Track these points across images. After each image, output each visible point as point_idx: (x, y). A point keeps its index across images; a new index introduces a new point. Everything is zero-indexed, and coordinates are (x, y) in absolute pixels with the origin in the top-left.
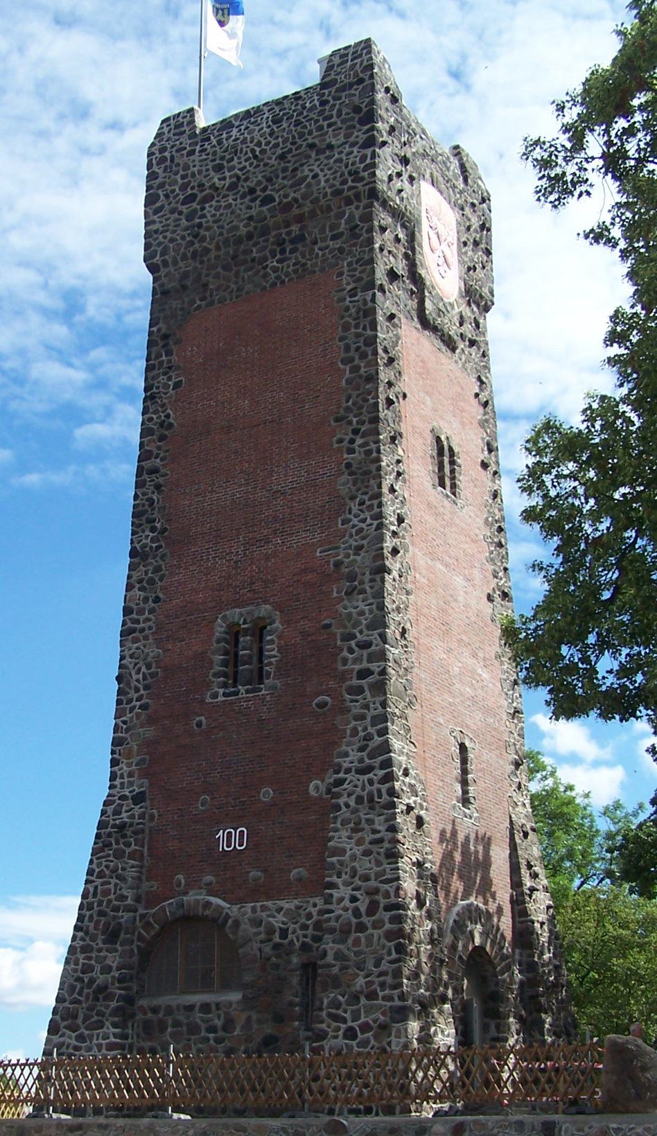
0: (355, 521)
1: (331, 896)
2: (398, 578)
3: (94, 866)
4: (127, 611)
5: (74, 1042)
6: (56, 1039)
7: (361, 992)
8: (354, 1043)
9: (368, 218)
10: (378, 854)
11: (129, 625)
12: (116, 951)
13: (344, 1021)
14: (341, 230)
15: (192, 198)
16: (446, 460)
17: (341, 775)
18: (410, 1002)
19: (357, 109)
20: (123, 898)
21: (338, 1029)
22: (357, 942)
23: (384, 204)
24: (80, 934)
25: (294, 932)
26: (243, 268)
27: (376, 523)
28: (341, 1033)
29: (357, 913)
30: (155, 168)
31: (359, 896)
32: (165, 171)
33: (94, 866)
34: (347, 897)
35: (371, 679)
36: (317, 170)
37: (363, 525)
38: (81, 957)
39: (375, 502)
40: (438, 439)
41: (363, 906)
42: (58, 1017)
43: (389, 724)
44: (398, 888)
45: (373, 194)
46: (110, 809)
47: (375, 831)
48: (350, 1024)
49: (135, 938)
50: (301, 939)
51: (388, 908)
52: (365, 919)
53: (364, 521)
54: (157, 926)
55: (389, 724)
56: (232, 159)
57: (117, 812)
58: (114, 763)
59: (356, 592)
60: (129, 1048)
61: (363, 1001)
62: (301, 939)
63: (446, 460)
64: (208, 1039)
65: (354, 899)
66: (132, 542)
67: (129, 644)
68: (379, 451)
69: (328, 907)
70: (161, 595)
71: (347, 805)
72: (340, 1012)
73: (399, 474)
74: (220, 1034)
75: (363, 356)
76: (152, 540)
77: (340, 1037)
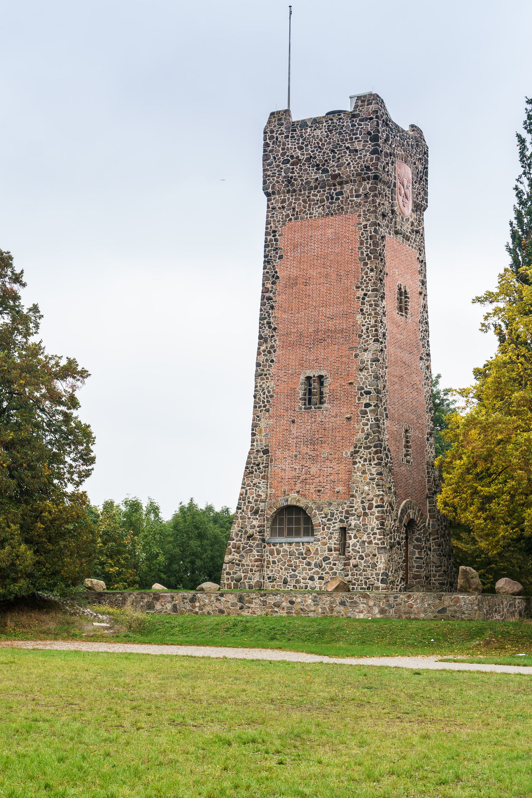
8: (363, 561)
13: (359, 552)
17: (357, 449)
25: (337, 514)
29: (364, 508)
30: (268, 141)
41: (366, 505)
47: (371, 474)
48: (361, 554)
52: (367, 511)
61: (366, 544)
62: (340, 518)
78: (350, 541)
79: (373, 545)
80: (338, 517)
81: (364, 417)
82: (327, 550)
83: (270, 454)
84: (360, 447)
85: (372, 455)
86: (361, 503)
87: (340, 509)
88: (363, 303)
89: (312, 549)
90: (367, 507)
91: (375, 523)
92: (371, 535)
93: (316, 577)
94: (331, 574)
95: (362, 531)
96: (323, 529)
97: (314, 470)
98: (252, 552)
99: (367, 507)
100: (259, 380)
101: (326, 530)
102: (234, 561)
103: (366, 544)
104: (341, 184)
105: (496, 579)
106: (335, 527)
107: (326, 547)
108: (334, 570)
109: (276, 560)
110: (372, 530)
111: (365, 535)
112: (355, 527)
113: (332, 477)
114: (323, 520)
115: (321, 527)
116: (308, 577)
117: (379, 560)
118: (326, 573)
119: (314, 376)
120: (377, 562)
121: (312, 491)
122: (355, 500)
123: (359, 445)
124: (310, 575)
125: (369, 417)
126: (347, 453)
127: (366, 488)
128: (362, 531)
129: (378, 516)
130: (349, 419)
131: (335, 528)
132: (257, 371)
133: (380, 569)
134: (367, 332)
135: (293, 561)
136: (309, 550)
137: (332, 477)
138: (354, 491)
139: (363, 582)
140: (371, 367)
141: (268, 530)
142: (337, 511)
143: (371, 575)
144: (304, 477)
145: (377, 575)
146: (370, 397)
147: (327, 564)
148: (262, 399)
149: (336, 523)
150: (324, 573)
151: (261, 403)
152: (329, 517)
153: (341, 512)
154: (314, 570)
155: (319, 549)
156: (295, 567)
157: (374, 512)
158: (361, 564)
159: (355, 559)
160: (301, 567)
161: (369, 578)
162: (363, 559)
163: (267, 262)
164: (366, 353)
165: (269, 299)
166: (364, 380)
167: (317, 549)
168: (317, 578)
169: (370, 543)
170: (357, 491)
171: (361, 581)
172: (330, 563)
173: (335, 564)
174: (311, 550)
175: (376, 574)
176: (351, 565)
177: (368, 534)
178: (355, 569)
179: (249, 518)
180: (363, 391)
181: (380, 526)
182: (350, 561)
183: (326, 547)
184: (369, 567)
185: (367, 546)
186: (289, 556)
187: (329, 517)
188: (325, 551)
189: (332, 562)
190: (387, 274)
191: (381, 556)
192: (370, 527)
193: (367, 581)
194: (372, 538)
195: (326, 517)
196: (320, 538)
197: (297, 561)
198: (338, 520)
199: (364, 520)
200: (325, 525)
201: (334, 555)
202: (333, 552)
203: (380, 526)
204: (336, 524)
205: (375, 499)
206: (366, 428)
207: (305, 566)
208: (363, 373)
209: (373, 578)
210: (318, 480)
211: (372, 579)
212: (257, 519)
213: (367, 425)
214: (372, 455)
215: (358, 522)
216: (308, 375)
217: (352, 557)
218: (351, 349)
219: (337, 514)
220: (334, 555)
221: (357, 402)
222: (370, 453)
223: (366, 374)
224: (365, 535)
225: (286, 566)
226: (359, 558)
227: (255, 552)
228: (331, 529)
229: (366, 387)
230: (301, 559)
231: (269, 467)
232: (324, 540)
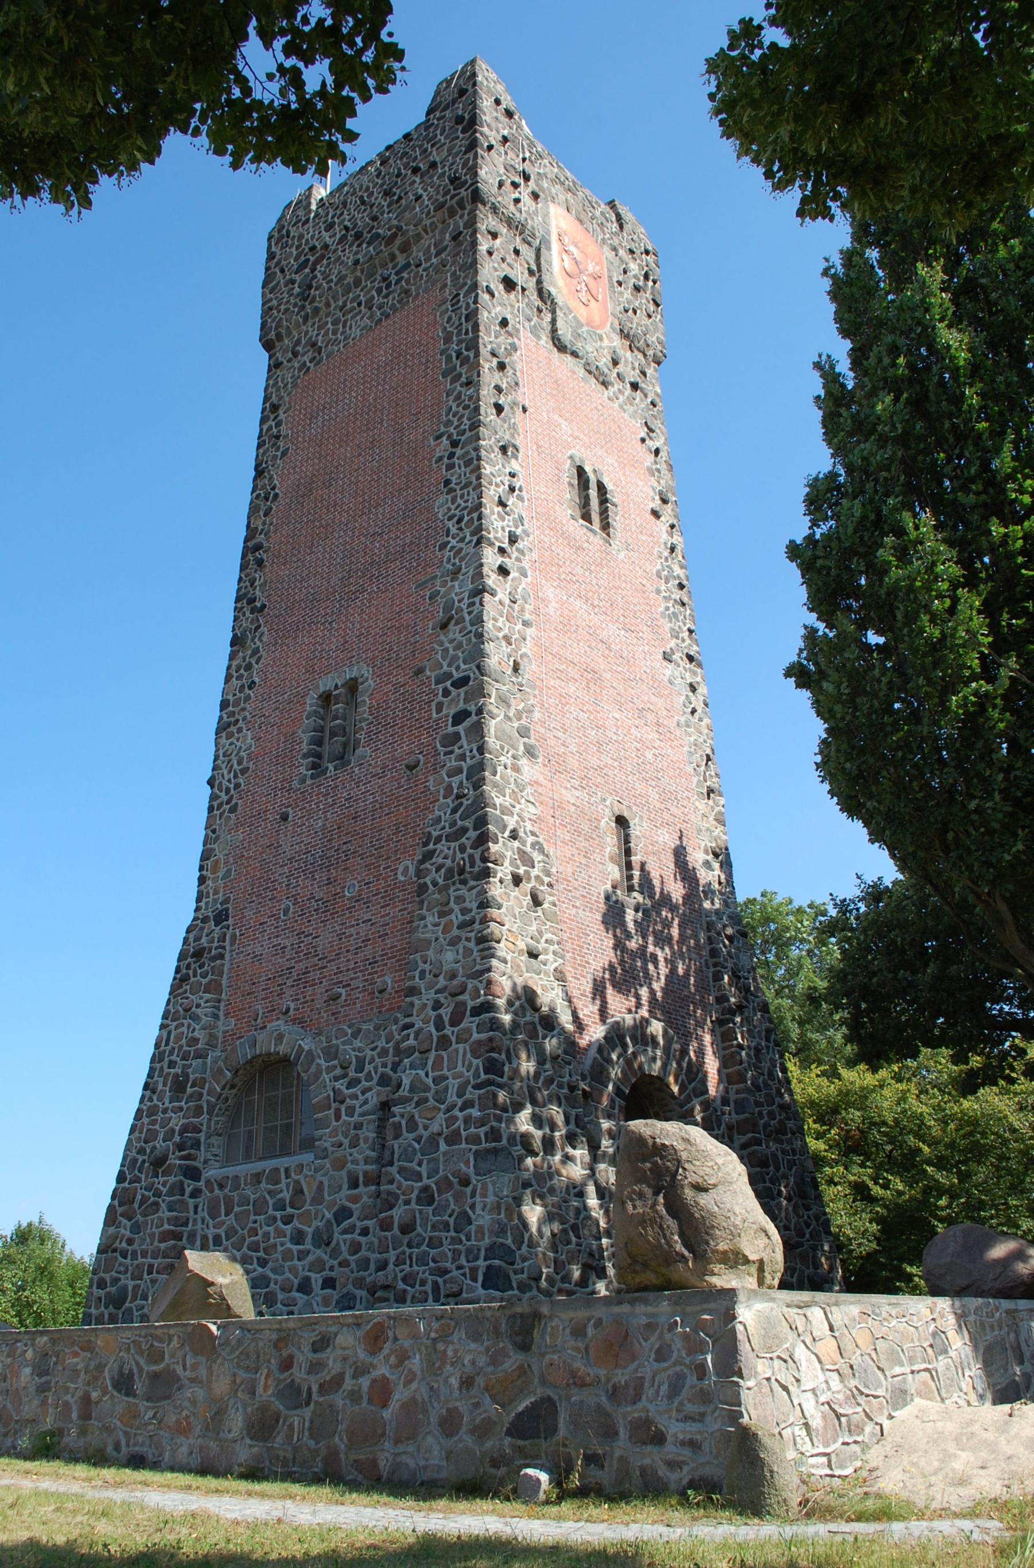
0: (453, 542)
1: (412, 1004)
2: (507, 602)
3: (171, 1007)
4: (224, 705)
5: (128, 1234)
6: (112, 1230)
7: (440, 1134)
8: (430, 1209)
9: (472, 224)
10: (468, 939)
11: (225, 719)
12: (181, 1109)
13: (419, 1177)
14: (446, 243)
15: (305, 264)
16: (593, 493)
17: (431, 846)
18: (504, 1141)
19: (459, 120)
20: (196, 1040)
21: (412, 1189)
22: (438, 1064)
23: (495, 209)
24: (148, 1093)
25: (372, 1060)
26: (349, 316)
27: (475, 539)
28: (414, 1196)
29: (439, 1025)
30: (273, 249)
31: (443, 1000)
32: (282, 248)
33: (171, 1007)
34: (430, 1004)
35: (467, 723)
36: (420, 191)
37: (461, 545)
38: (146, 1120)
39: (475, 515)
40: (581, 471)
41: (446, 1013)
42: (116, 1202)
43: (487, 774)
44: (489, 983)
45: (477, 197)
46: (191, 936)
47: (464, 911)
48: (426, 1181)
49: (205, 1092)
50: (380, 1070)
51: (477, 1011)
52: (448, 1031)
53: (462, 540)
54: (228, 1073)
55: (487, 774)
56: (342, 214)
57: (197, 939)
58: (202, 880)
59: (453, 622)
60: (188, 1237)
61: (443, 1146)
62: (380, 1070)
63: (593, 493)
64: (275, 1219)
65: (437, 1005)
66: (234, 629)
67: (223, 741)
68: (479, 458)
69: (408, 1020)
70: (256, 680)
71: (435, 884)
72: (414, 1165)
73: (512, 489)
74: (289, 1210)
75: (465, 361)
76: (252, 622)
77: (414, 1201)
78: (396, 1144)
79: (464, 1145)
80: (376, 1068)
81: (451, 752)
82: (345, 1186)
83: (231, 921)
84: (438, 840)
85: (469, 851)
86: (434, 1009)
87: (382, 1043)
88: (450, 467)
89: (309, 1184)
90: (446, 1019)
91: (470, 1065)
92: (456, 1112)
93: (316, 1279)
94: (353, 1265)
95: (432, 1102)
96: (338, 1117)
97: (325, 942)
98: (157, 1211)
99: (446, 1019)
100: (223, 741)
101: (344, 1117)
102: (117, 1244)
103: (443, 1146)
104: (405, 248)
105: (1024, 546)
106: (366, 1102)
107: (344, 1173)
108: (364, 1253)
109: (221, 1231)
110: (460, 1095)
111: (441, 1115)
112: (412, 1089)
113: (368, 952)
114: (338, 1085)
115: (332, 1111)
116: (296, 1282)
117: (478, 1199)
118: (340, 1264)
119: (336, 687)
120: (473, 1207)
121: (319, 1004)
122: (417, 1002)
123: (435, 834)
124: (301, 1273)
125: (465, 746)
126: (406, 869)
127: (449, 956)
128: (432, 1102)
129: (479, 1042)
130: (411, 768)
131: (366, 1108)
132: (221, 718)
133: (480, 1230)
134: (461, 529)
135: (260, 1232)
136: (302, 1192)
137: (368, 952)
138: (417, 973)
139: (428, 1288)
140: (470, 613)
141: (214, 1140)
142: (373, 1050)
143: (454, 1260)
144: (302, 965)
145: (472, 1254)
146: (466, 693)
147: (345, 1232)
148: (225, 783)
149: (370, 1089)
150: (336, 1263)
151: (223, 794)
152: (352, 1074)
153: (384, 1053)
154: (310, 1258)
155: (326, 1184)
156: (265, 1250)
157: (469, 1030)
158: (425, 1220)
159: (407, 1202)
160: (280, 1249)
161: (446, 1272)
162: (431, 1201)
163: (260, 471)
164: (456, 583)
165: (258, 547)
166: (451, 652)
167: (321, 1183)
168: (320, 1282)
169: (453, 1139)
170: (423, 973)
171: (423, 1283)
172: (350, 1230)
173: (365, 1232)
174: (305, 1190)
175: (469, 1251)
176: (396, 1229)
177: (448, 1110)
178: (406, 1239)
179: (165, 1111)
180: (448, 684)
181: (483, 1076)
182: (394, 1211)
183: (344, 1173)
184: (446, 1226)
185: (445, 1154)
186: (252, 1218)
187: (352, 1074)
188: (340, 1187)
189: (359, 1224)
190: (525, 410)
191: (485, 1186)
192: (453, 1084)
193: (440, 1280)
194: (460, 1123)
195: (345, 1076)
196: (326, 1144)
197: (271, 1229)
198: (376, 1078)
199: (438, 1064)
200: (342, 1102)
201: (365, 1199)
202: (361, 1189)
203: (483, 1076)
204: (368, 1095)
205: (470, 986)
206: (455, 781)
207: (289, 1245)
208: (451, 636)
209: (459, 1268)
210: (333, 966)
211: (455, 1273)
212: (181, 1109)
213: (459, 771)
214: (469, 851)
215: (422, 1073)
216: (322, 689)
217: (397, 1197)
218: (421, 586)
219: (372, 1060)
220: (365, 1199)
221: (435, 715)
222: (462, 849)
223: (458, 636)
224: (441, 1115)
225: (245, 1249)
226: (419, 1201)
227: (164, 1213)
228: (358, 1111)
229: (458, 668)
230: (279, 1223)
231: (227, 957)
232: (340, 1153)
